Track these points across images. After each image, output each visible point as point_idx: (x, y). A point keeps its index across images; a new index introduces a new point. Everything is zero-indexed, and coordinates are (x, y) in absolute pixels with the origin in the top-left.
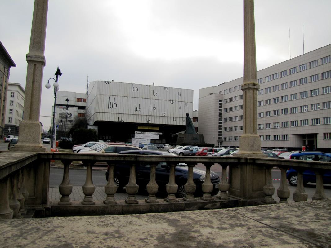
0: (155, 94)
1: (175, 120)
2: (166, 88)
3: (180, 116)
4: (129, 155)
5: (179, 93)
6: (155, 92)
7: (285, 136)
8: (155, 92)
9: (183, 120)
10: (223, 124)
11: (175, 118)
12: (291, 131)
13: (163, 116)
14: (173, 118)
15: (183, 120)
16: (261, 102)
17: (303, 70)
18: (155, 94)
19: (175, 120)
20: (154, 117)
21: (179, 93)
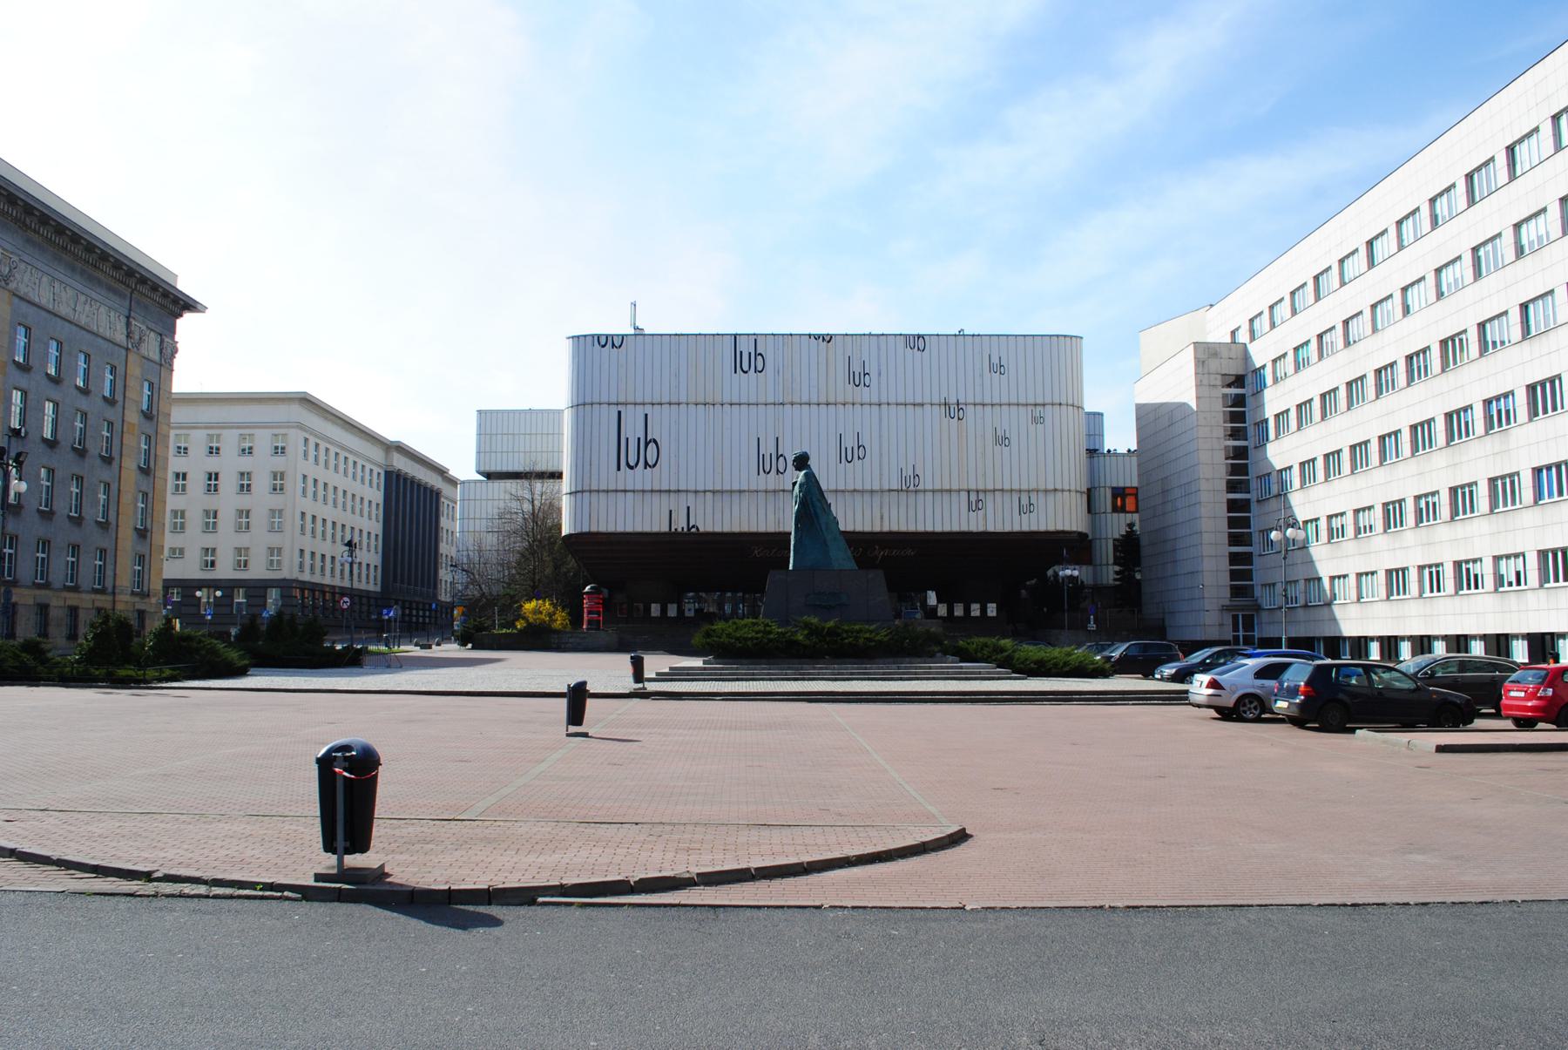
1: (975, 506)
2: (916, 342)
5: (995, 360)
6: (857, 368)
8: (857, 368)
9: (1025, 501)
13: (910, 487)
14: (964, 495)
18: (858, 379)
19: (975, 506)
20: (858, 497)
21: (995, 360)
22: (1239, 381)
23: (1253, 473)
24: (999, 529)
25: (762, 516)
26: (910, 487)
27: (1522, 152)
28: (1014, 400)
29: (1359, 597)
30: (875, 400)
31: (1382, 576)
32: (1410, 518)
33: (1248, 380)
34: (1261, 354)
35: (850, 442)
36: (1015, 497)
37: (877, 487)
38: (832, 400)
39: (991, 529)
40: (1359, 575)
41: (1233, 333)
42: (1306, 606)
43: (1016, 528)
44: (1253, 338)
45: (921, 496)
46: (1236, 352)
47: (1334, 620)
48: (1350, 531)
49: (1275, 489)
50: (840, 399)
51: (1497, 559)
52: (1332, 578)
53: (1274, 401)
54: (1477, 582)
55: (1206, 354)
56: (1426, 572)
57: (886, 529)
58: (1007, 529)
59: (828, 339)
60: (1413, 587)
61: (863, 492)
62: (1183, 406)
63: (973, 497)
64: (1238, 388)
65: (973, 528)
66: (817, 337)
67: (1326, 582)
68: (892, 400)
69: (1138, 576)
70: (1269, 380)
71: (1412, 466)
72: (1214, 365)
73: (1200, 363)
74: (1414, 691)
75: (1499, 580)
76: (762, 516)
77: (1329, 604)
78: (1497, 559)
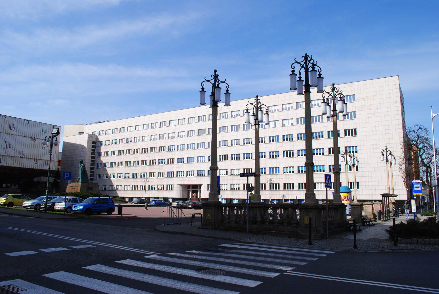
0: (12, 128)
1: (36, 163)
2: (27, 121)
3: (28, 156)
4: (239, 243)
5: (44, 129)
6: (12, 125)
7: (170, 187)
8: (12, 125)
9: (46, 163)
10: (95, 170)
11: (36, 161)
12: (177, 182)
13: (21, 157)
14: (33, 160)
15: (46, 163)
16: (225, 157)
17: (347, 131)
18: (12, 128)
19: (36, 163)
20: (8, 157)
21: (44, 129)
22: (94, 143)
23: (95, 162)
24: (40, 168)
25: (8, 162)
26: (21, 157)
27: (171, 122)
28: (23, 135)
29: (124, 189)
30: (15, 134)
31: (131, 186)
32: (139, 177)
33: (97, 143)
34: (101, 138)
35: (8, 143)
36: (45, 161)
37: (13, 155)
38: (4, 132)
39: (38, 168)
40: (125, 185)
41: (93, 132)
42: (109, 190)
43: (44, 169)
44: (99, 134)
45: (23, 159)
46: (95, 137)
47: (117, 193)
48: (124, 177)
49: (102, 166)
50: (7, 132)
51: (158, 185)
52: (117, 185)
53: (103, 149)
54: (153, 189)
55: (90, 136)
56: (142, 186)
57: (14, 166)
58: (42, 169)
59: (5, 116)
60: (139, 189)
61: (9, 156)
62: (82, 146)
63: (35, 161)
64: (95, 144)
65: (34, 168)
66: (3, 116)
67: (115, 186)
68: (19, 135)
69: (59, 181)
70: (104, 144)
71: (141, 168)
72: (91, 139)
73: (89, 138)
74: (84, 208)
75: (158, 189)
76: (8, 162)
77: (116, 190)
78: (158, 185)
